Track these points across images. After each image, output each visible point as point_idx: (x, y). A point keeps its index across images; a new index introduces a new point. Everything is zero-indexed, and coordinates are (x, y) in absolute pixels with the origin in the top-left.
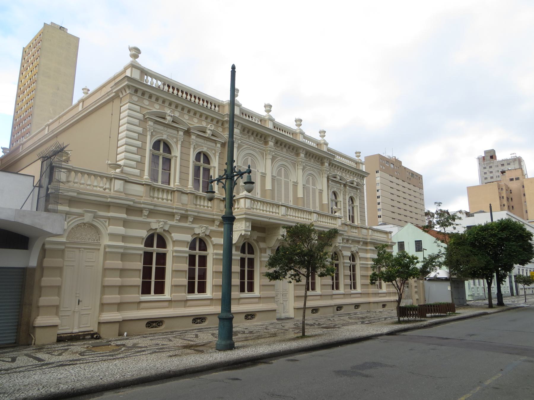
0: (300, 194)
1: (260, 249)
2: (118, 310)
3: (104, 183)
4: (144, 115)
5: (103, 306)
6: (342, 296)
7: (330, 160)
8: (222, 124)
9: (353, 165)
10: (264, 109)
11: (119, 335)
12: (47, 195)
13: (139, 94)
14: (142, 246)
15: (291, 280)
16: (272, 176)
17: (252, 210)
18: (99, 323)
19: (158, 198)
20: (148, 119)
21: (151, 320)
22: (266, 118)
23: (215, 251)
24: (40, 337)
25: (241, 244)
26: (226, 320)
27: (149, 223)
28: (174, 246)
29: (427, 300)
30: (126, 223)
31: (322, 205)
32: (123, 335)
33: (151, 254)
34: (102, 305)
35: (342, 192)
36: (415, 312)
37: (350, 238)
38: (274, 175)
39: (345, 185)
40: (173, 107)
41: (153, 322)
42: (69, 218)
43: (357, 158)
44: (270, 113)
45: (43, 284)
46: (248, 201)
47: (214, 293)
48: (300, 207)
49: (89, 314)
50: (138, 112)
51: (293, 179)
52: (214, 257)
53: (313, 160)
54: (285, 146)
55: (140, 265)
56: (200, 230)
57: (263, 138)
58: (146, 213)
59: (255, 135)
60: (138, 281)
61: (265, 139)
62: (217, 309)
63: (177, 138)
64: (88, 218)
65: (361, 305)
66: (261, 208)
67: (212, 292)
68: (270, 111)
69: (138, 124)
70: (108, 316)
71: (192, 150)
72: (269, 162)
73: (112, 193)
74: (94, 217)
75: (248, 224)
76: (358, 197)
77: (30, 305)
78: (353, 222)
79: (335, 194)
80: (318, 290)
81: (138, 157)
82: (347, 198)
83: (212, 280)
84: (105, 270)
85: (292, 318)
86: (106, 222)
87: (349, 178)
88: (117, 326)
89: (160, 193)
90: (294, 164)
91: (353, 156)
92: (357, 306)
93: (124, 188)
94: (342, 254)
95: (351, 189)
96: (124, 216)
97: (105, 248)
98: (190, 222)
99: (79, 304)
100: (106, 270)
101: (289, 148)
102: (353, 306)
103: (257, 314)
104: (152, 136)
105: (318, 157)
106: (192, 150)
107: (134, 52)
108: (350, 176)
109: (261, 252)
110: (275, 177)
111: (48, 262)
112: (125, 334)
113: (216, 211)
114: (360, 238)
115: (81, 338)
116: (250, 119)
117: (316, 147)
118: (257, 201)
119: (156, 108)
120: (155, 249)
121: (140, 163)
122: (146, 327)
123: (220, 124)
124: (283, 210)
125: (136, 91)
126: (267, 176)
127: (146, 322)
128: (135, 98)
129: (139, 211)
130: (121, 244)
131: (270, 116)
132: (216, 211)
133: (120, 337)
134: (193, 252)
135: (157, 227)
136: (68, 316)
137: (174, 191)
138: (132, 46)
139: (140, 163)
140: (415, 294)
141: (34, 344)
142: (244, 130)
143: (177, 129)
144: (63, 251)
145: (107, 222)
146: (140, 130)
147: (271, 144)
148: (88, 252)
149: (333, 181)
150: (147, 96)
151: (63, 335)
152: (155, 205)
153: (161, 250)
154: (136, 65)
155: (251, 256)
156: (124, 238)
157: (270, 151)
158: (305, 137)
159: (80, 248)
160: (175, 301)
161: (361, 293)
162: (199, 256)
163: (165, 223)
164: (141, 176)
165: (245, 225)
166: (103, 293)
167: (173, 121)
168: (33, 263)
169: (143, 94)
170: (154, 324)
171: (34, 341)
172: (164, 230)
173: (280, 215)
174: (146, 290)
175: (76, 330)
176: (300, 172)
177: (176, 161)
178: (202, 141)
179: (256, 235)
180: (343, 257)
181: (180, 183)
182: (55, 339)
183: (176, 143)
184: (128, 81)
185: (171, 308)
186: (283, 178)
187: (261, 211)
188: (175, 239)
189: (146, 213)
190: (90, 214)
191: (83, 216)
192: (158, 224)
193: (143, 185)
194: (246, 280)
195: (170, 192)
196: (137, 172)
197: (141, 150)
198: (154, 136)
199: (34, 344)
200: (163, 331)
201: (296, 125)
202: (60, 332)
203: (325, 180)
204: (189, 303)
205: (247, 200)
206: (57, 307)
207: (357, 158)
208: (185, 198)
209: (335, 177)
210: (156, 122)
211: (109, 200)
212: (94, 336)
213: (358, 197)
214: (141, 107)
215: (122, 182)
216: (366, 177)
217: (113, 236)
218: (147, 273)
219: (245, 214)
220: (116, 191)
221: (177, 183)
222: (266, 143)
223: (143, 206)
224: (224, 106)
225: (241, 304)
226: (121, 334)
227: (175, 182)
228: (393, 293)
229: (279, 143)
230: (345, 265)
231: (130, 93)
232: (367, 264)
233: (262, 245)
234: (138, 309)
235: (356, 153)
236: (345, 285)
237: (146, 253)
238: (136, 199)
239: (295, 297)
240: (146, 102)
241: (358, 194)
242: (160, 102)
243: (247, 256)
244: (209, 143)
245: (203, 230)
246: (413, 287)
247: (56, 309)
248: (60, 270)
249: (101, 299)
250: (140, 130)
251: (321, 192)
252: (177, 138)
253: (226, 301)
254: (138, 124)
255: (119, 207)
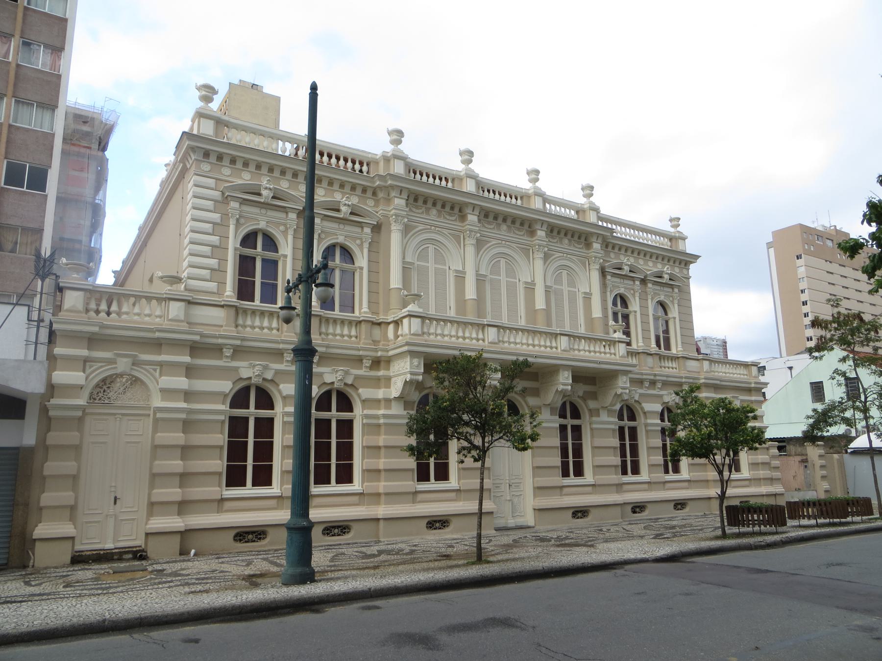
0: (540, 303)
1: (590, 410)
2: (180, 513)
3: (742, 371)
4: (223, 194)
5: (154, 507)
6: (686, 484)
7: (604, 238)
8: (374, 194)
9: (665, 243)
10: (527, 177)
11: (181, 554)
12: (52, 334)
13: (213, 159)
14: (225, 407)
15: (463, 458)
16: (546, 286)
17: (572, 352)
18: (147, 534)
19: (253, 327)
20: (229, 198)
21: (248, 530)
22: (530, 192)
23: (365, 412)
24: (41, 555)
25: (559, 405)
26: (301, 533)
27: (236, 369)
28: (363, 409)
29: (851, 491)
30: (190, 371)
31: (590, 321)
32: (189, 553)
33: (329, 421)
34: (152, 505)
35: (637, 295)
36: (759, 517)
37: (658, 378)
38: (548, 284)
39: (644, 281)
40: (347, 189)
41: (248, 533)
42: (91, 367)
43: (672, 230)
44: (537, 184)
45: (46, 473)
46: (416, 322)
47: (365, 484)
48: (541, 327)
49: (133, 519)
50: (212, 189)
51: (525, 276)
52: (364, 421)
53: (566, 241)
54: (566, 235)
55: (221, 438)
56: (249, 370)
57: (456, 210)
58: (228, 352)
59: (439, 206)
60: (219, 464)
61: (529, 227)
62: (284, 515)
63: (285, 225)
64: (123, 365)
65: (690, 503)
66: (524, 341)
67: (363, 482)
68: (537, 180)
69: (212, 208)
70: (160, 523)
71: (650, 301)
72: (470, 251)
73: (166, 325)
74: (133, 364)
75: (416, 361)
76: (676, 302)
77: (27, 505)
78: (668, 347)
79: (662, 305)
80: (745, 472)
81: (213, 262)
82: (651, 305)
83: (282, 462)
84: (155, 448)
85: (529, 527)
86: (155, 370)
87: (650, 267)
88: (619, 509)
89: (257, 319)
90: (526, 251)
91: (667, 227)
92: (680, 504)
93: (187, 314)
94: (642, 408)
95: (658, 288)
96: (187, 359)
97: (155, 414)
98: (366, 367)
99: (115, 503)
100: (157, 449)
101: (572, 236)
102: (570, 513)
103: (648, 505)
104: (238, 224)
105: (578, 234)
106: (650, 301)
107: (204, 93)
108: (655, 264)
109: (591, 416)
110: (550, 287)
111: (54, 437)
112: (193, 552)
113: (364, 344)
114: (681, 377)
115: (115, 557)
116: (450, 185)
117: (576, 217)
118: (580, 338)
119: (246, 178)
120: (252, 412)
121: (217, 273)
122: (235, 540)
123: (369, 194)
124: (564, 342)
125: (207, 154)
126: (593, 297)
127: (234, 532)
128: (206, 167)
129: (216, 350)
130: (184, 405)
131: (591, 203)
132: (364, 344)
133: (182, 558)
134: (622, 423)
135: (334, 380)
136: (98, 522)
137: (360, 322)
138: (201, 82)
139: (217, 273)
140: (753, 478)
141: (33, 566)
142: (552, 231)
143: (361, 225)
144: (81, 420)
145: (158, 371)
146: (216, 217)
147: (541, 233)
148: (129, 420)
149: (614, 275)
150: (264, 170)
151: (83, 554)
152: (243, 339)
153: (345, 415)
154: (205, 112)
155: (576, 422)
156: (188, 395)
157: (539, 246)
158: (546, 200)
159: (114, 414)
160: (600, 485)
161: (689, 481)
162: (629, 428)
163: (347, 373)
164: (220, 292)
165: (411, 363)
166: (152, 486)
167: (351, 213)
168: (29, 439)
169: (220, 158)
170: (250, 536)
171: (32, 561)
172: (346, 384)
173: (486, 342)
174: (235, 478)
175: (110, 545)
176: (539, 264)
177: (675, 322)
178: (335, 225)
179: (582, 389)
180: (645, 413)
181: (369, 308)
182: (68, 559)
183: (361, 247)
184: (189, 139)
185: (282, 509)
186: (503, 278)
187: (587, 353)
188: (284, 394)
189: (228, 352)
190: (125, 360)
191: (116, 363)
192: (251, 371)
193: (222, 306)
194: (629, 458)
195: (354, 324)
196: (212, 286)
197: (218, 250)
198: (243, 224)
199: (33, 566)
200: (266, 548)
201: (584, 196)
202: (78, 547)
203: (595, 276)
204: (227, 505)
205: (412, 319)
206: (73, 508)
207: (672, 230)
208: (650, 360)
209: (620, 269)
210: (244, 202)
211: (158, 335)
212: (139, 555)
213: (676, 302)
214: (216, 179)
215: (182, 304)
216: (692, 262)
217: (167, 393)
218: (236, 451)
219: (407, 344)
220: (171, 320)
221: (365, 308)
222: (588, 245)
223: (220, 341)
224: (377, 162)
225: (420, 502)
226: (184, 552)
227: (361, 308)
228: (764, 479)
229: (487, 215)
230: (649, 428)
231: (195, 159)
232: (376, 417)
233: (592, 404)
234: (219, 510)
235: (671, 220)
236: (652, 466)
237: (233, 420)
238: (207, 331)
239: (534, 488)
240: (226, 171)
241: (675, 295)
242: (252, 168)
243: (570, 422)
244: (348, 228)
245: (339, 376)
246: (817, 467)
247: (72, 511)
248: (77, 449)
249: (149, 495)
250: (216, 217)
251: (588, 297)
252: (285, 225)
253: (301, 501)
254: (212, 208)
255: (175, 345)
